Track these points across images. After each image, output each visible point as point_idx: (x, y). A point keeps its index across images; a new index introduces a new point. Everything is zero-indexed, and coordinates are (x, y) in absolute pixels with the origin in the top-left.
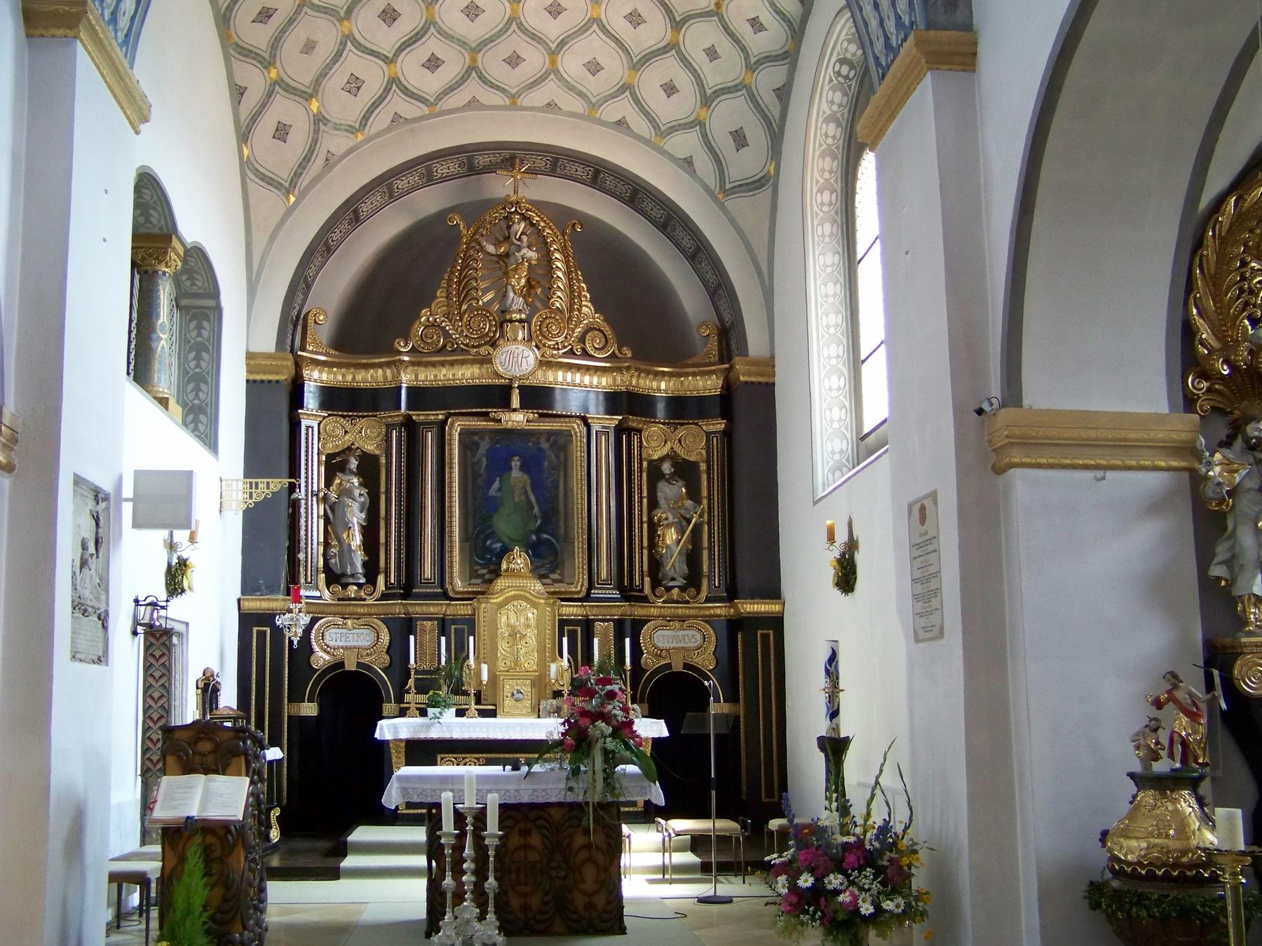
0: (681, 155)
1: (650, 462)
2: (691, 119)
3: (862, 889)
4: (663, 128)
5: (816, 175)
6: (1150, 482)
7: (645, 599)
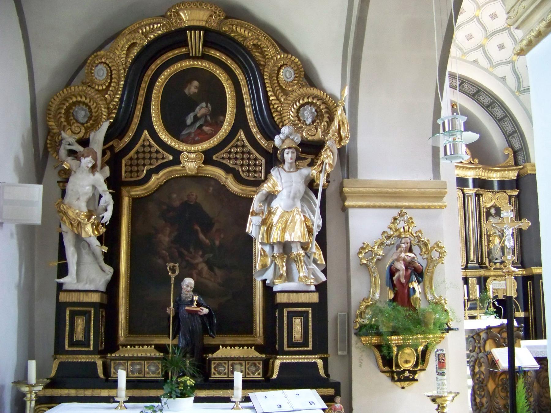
0: (500, 75)
1: (487, 208)
2: (509, 60)
4: (494, 64)
7: (486, 268)
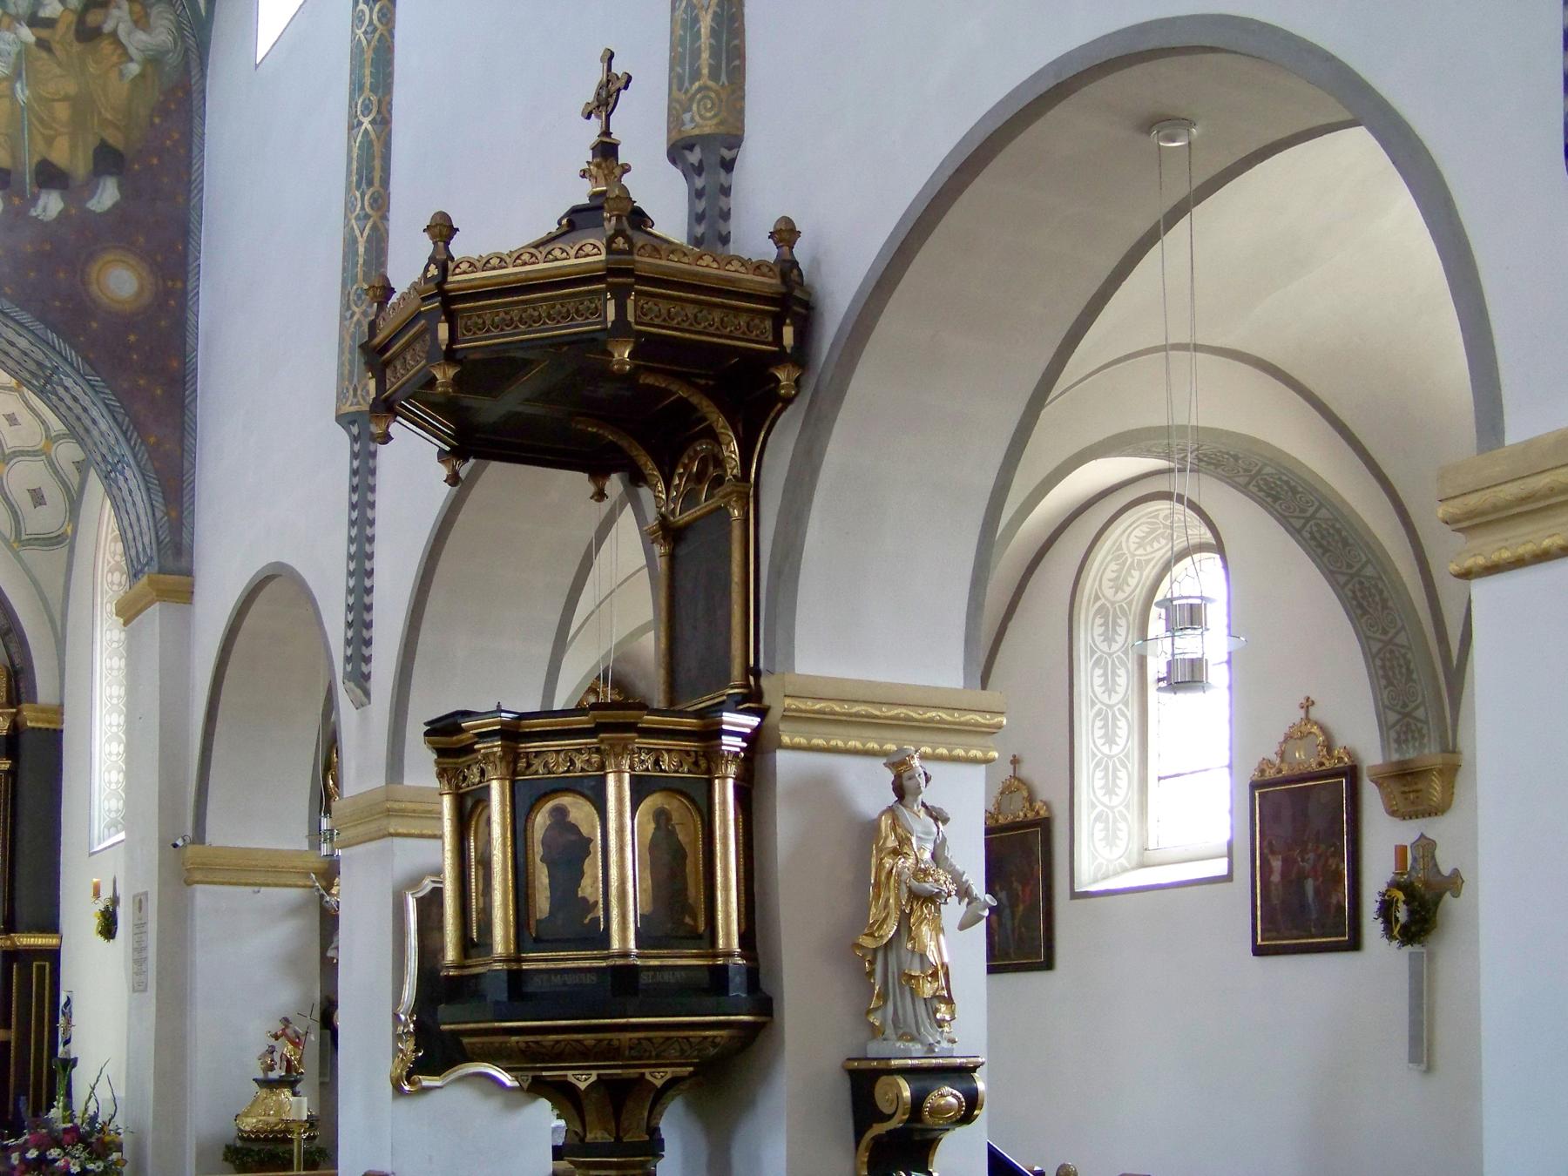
3: (74, 1157)
5: (108, 556)
6: (293, 894)
